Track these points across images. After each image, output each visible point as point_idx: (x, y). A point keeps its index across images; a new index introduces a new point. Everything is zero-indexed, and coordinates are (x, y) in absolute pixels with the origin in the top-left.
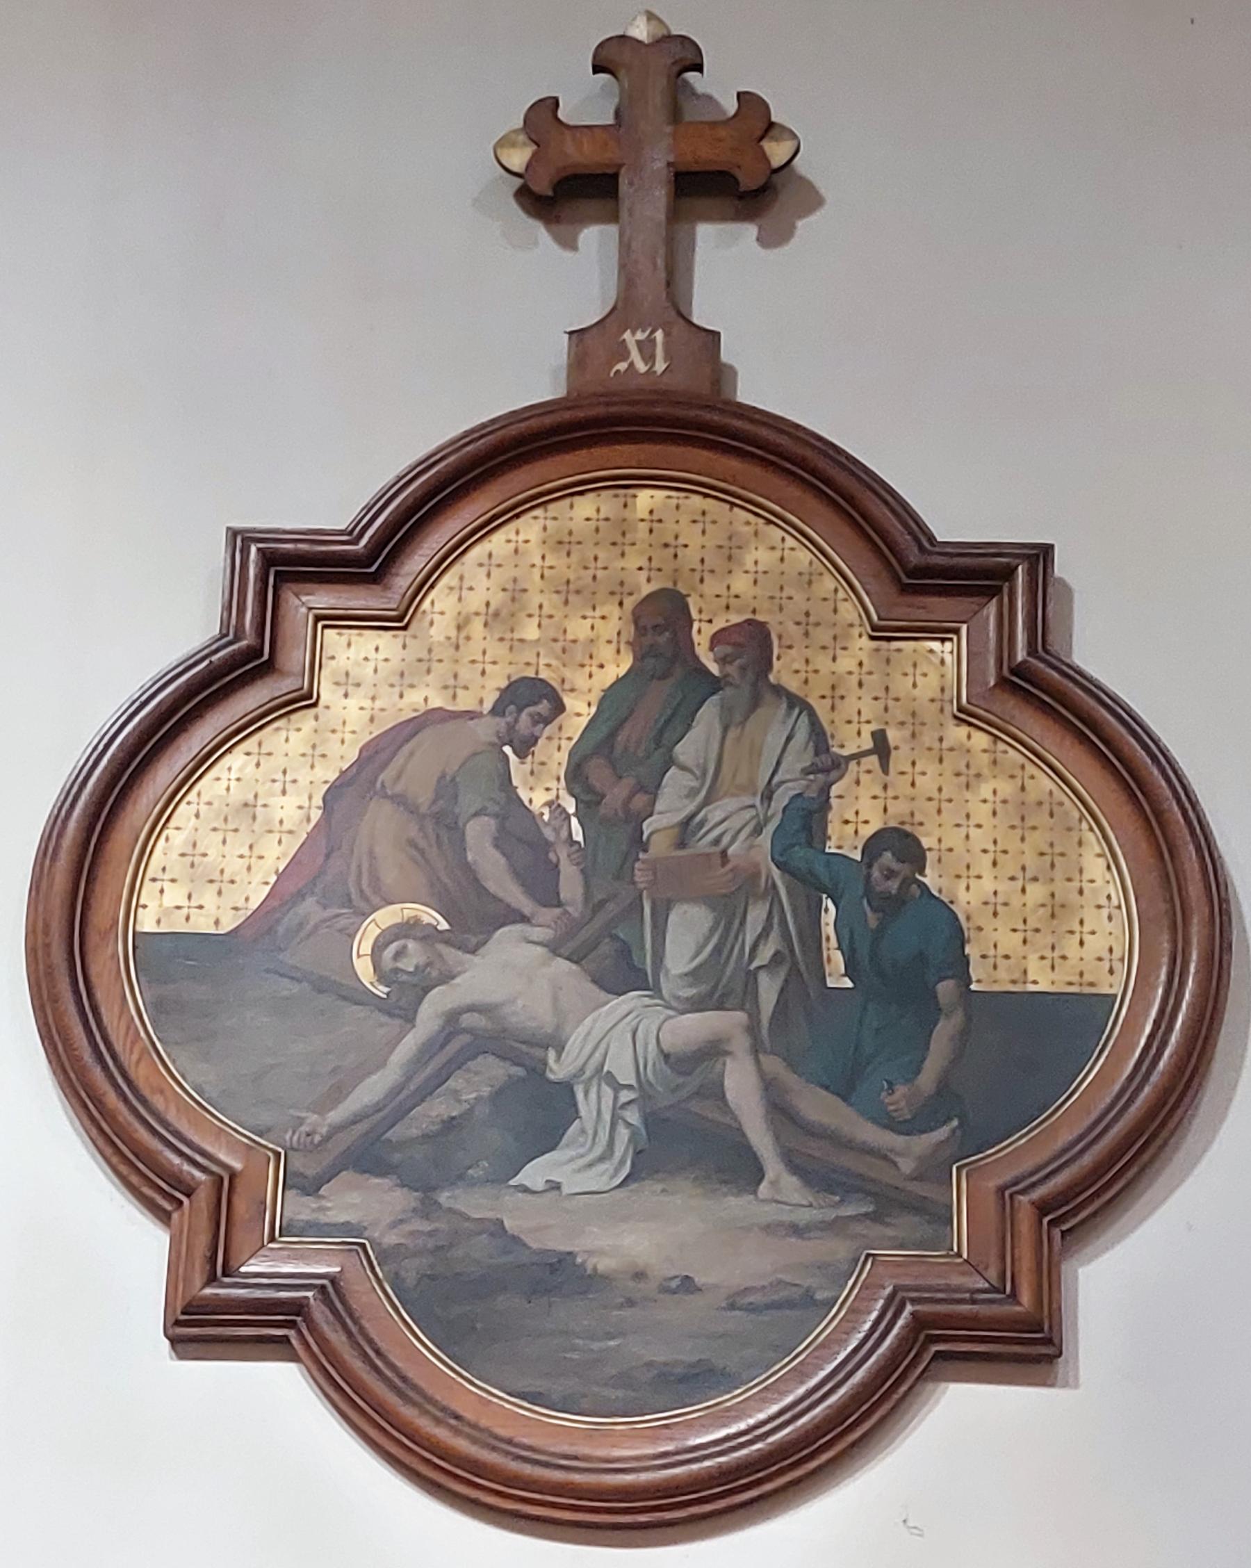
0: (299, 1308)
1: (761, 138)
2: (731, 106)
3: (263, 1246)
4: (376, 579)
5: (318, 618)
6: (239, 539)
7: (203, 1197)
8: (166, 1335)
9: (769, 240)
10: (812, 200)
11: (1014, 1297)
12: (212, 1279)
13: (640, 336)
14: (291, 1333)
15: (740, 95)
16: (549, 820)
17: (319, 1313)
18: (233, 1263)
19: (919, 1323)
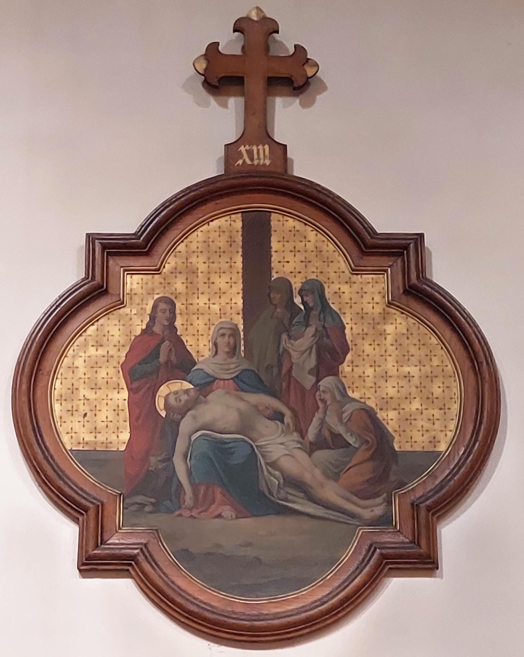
0: (133, 558)
1: (304, 65)
2: (292, 50)
3: (117, 532)
4: (147, 254)
5: (125, 271)
6: (91, 238)
7: (92, 513)
8: (78, 568)
9: (305, 105)
10: (323, 88)
11: (419, 545)
12: (97, 547)
13: (247, 147)
14: (130, 568)
15: (296, 46)
16: (156, 499)
17: (141, 558)
18: (106, 538)
19: (383, 556)
